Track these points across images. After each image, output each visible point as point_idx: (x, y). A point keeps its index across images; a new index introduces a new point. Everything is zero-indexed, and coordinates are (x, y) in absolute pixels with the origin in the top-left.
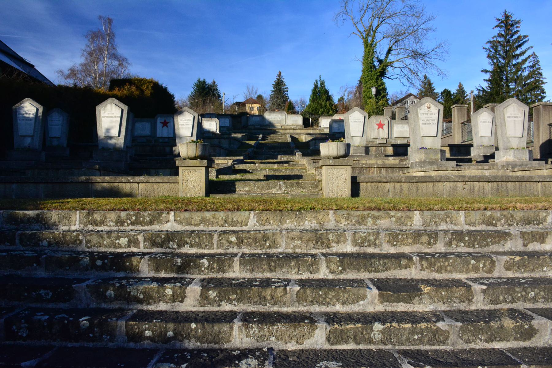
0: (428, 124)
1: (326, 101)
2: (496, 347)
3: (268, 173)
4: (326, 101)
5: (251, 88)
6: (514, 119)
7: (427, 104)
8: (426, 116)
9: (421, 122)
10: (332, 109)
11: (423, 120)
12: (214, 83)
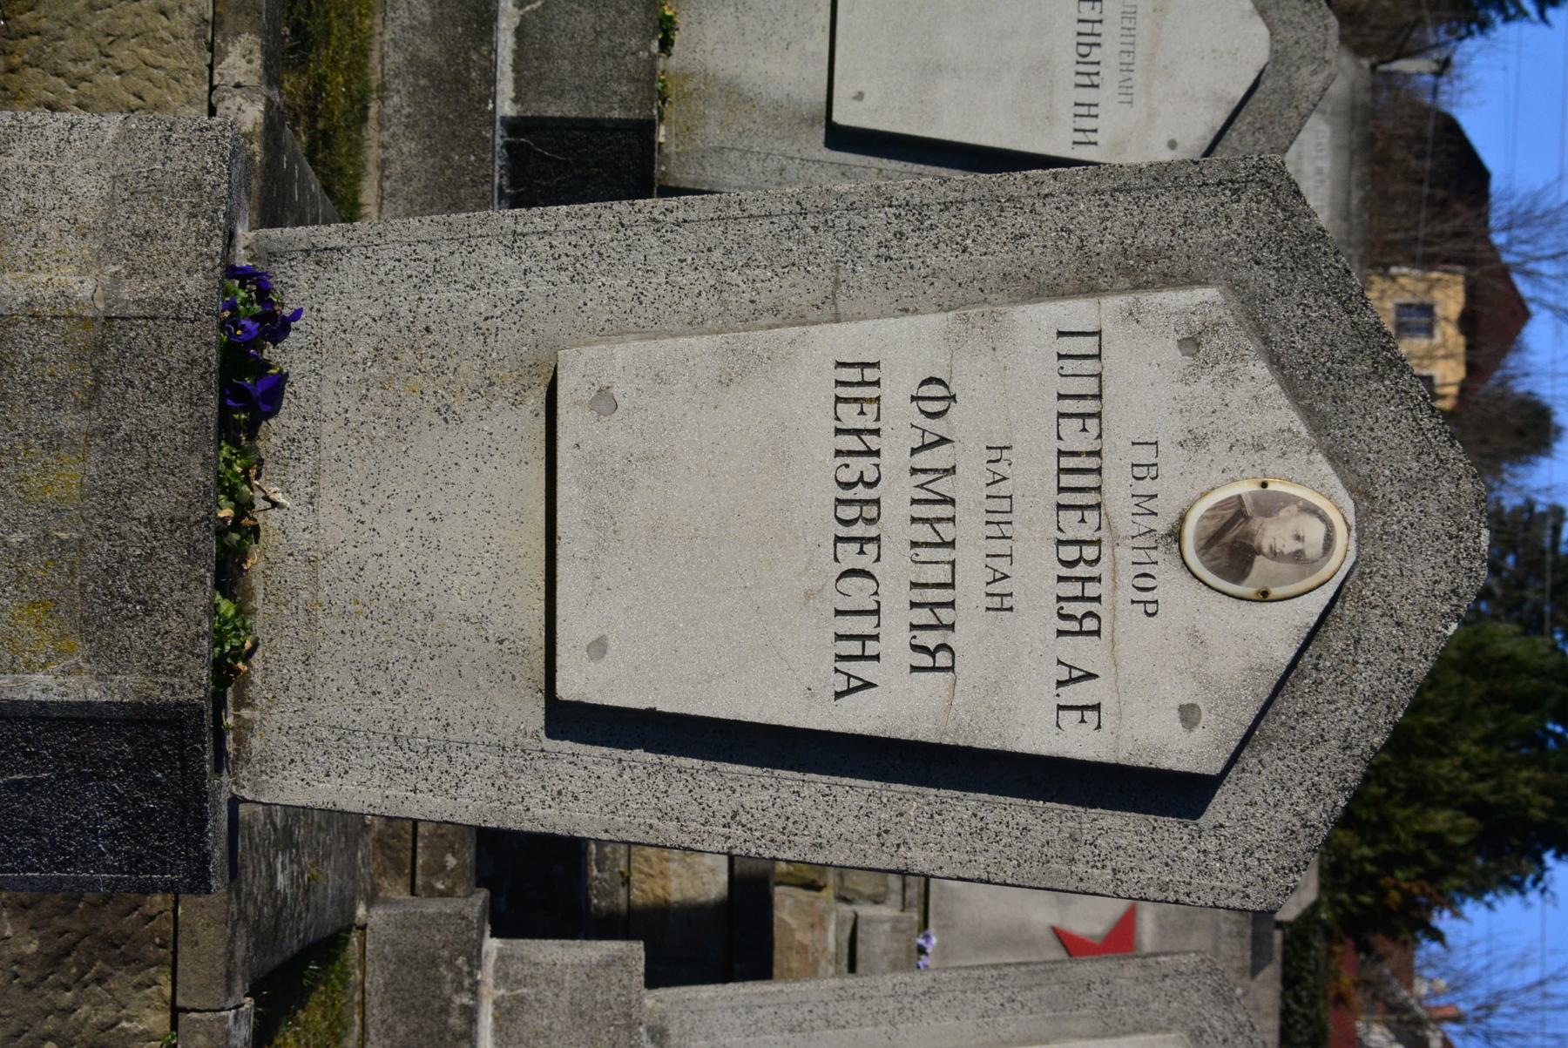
0: (857, 508)
1: (1476, 808)
4: (1476, 808)
7: (1314, 512)
8: (1034, 478)
9: (906, 345)
10: (1388, 862)
11: (936, 395)
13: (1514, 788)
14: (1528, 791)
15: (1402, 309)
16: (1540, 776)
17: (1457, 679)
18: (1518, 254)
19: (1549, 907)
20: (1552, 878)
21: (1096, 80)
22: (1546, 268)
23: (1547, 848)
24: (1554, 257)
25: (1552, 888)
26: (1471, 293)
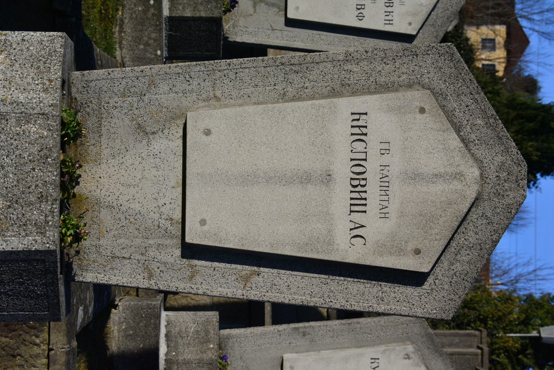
2: (168, 6)
6: (343, 171)
13: (526, 148)
14: (531, 149)
15: (484, 41)
16: (535, 144)
17: (506, 110)
18: (525, 12)
19: (538, 193)
20: (540, 183)
22: (536, 17)
23: (538, 172)
24: (538, 13)
25: (540, 186)
26: (508, 33)
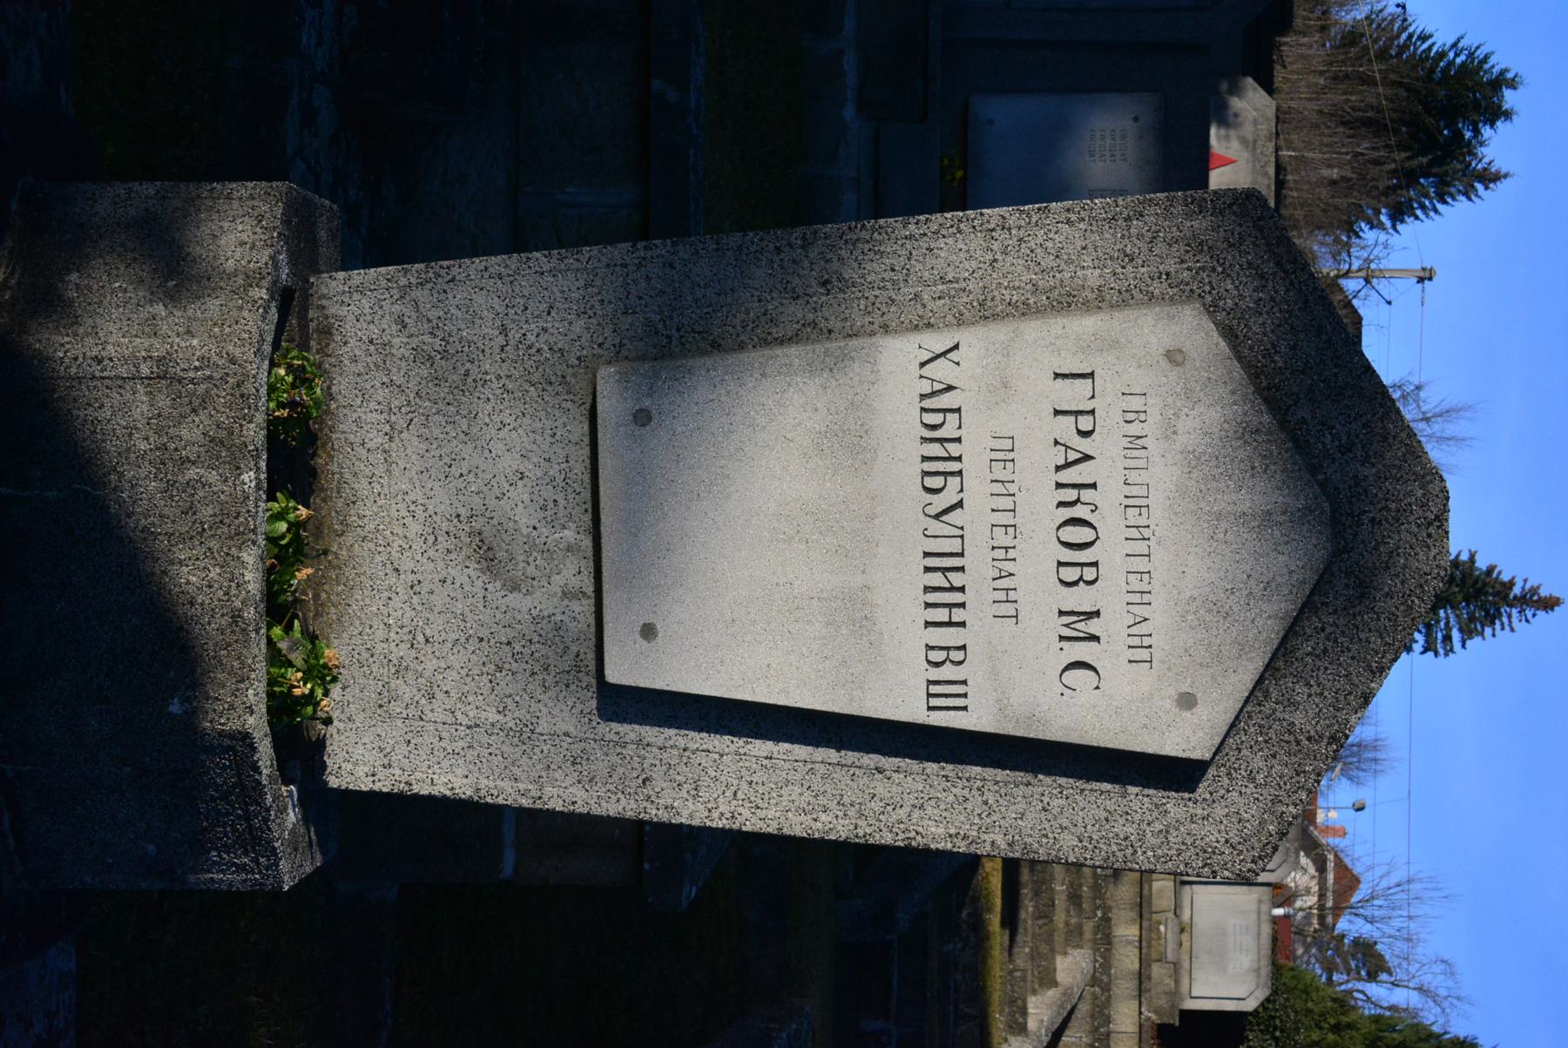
3: (1175, 805)
5: (1451, 429)
12: (1490, 178)
21: (958, 615)
